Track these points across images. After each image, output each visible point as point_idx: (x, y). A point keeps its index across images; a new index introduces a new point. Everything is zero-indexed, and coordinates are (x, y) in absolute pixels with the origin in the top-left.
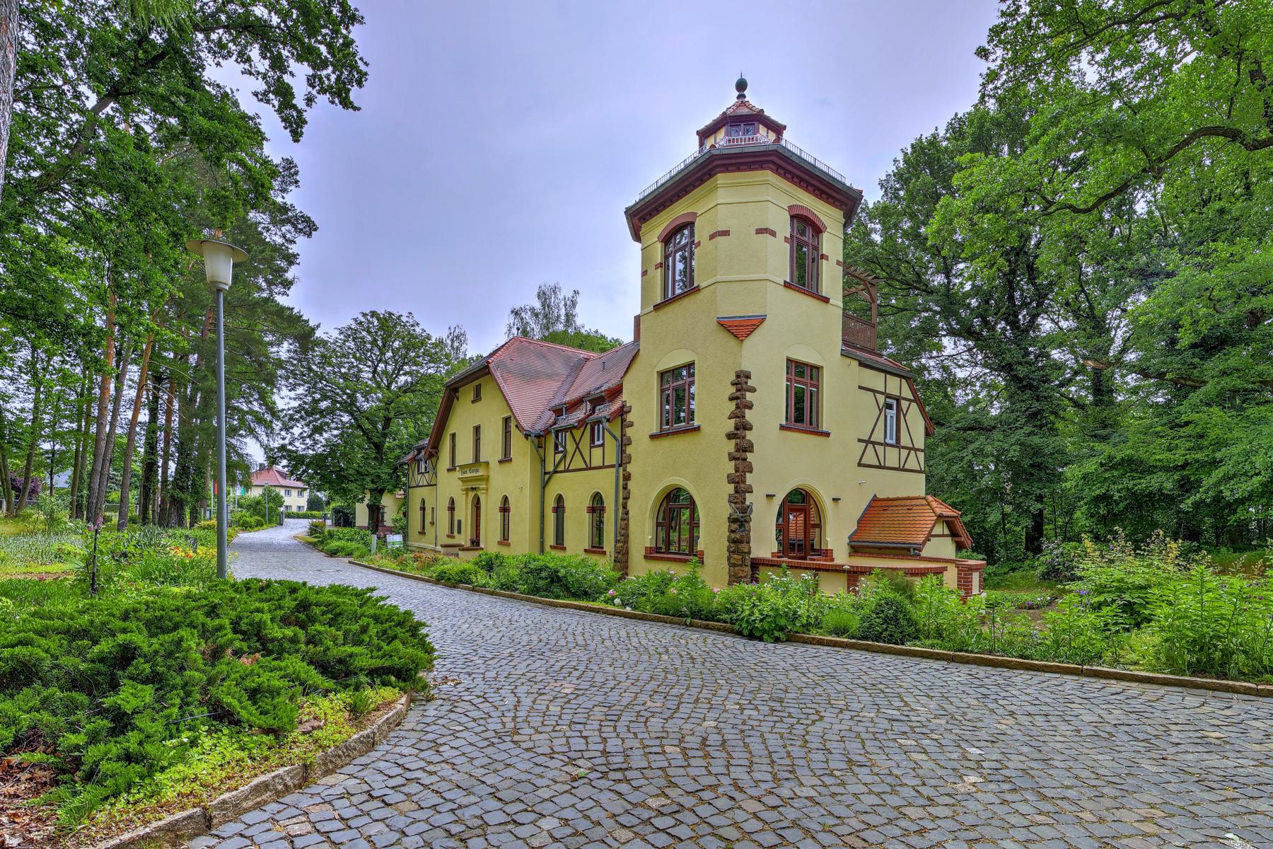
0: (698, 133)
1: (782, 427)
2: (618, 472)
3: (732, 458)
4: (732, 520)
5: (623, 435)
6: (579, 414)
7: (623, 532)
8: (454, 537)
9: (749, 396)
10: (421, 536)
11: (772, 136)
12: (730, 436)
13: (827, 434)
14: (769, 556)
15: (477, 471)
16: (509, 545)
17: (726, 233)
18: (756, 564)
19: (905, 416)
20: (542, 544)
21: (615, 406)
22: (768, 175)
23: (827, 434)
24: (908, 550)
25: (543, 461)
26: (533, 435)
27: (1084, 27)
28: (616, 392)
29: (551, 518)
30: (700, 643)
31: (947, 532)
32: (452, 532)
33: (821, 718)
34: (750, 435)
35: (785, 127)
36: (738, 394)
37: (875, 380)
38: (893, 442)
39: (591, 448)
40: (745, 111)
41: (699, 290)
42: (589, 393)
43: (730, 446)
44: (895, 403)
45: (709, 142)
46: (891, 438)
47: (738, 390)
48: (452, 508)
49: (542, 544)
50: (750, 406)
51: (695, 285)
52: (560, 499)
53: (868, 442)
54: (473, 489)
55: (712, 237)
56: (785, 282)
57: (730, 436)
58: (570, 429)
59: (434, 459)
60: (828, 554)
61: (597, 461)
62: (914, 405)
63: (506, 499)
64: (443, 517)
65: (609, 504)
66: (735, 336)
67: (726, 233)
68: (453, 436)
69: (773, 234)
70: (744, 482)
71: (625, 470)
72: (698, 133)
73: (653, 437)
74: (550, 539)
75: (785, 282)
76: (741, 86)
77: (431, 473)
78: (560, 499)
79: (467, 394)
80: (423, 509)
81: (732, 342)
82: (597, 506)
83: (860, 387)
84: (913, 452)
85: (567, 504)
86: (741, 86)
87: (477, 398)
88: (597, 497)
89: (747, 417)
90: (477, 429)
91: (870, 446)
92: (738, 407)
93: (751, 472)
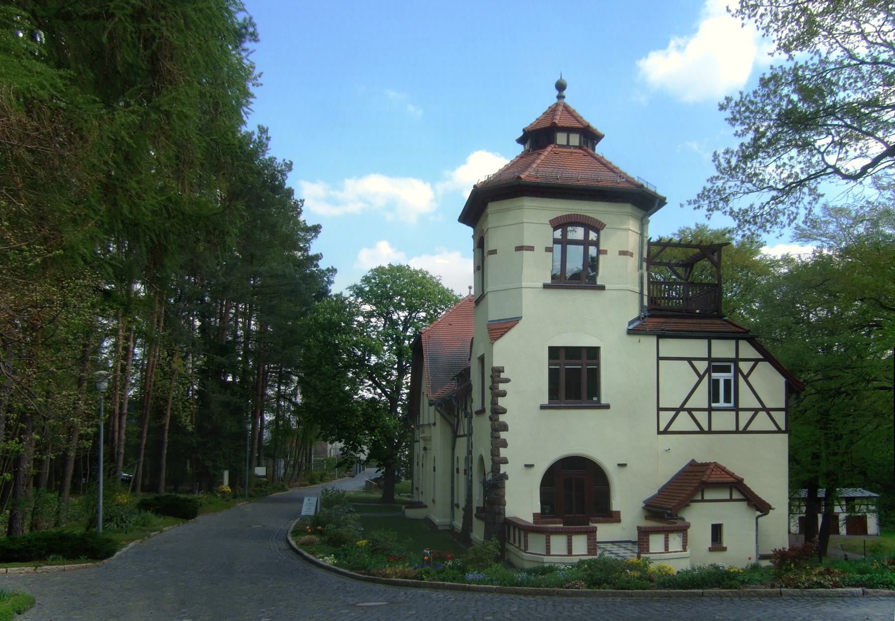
1: (543, 407)
9: (502, 387)
13: (607, 407)
23: (607, 407)
38: (731, 405)
46: (727, 400)
50: (504, 394)
76: (561, 87)
86: (561, 87)
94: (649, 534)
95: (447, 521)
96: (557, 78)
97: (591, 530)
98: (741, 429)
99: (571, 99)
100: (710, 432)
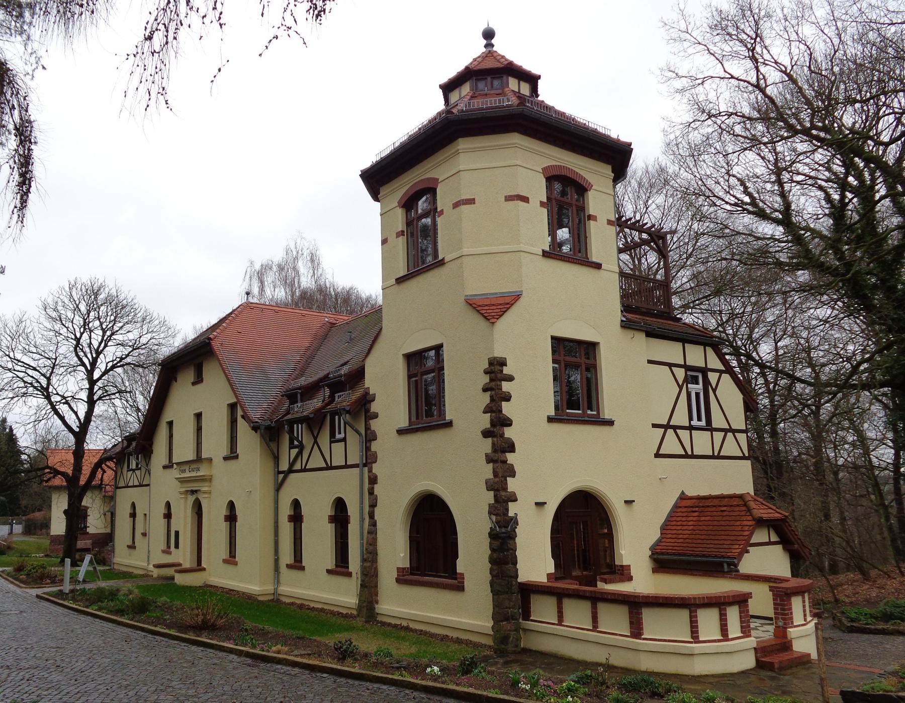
0: (441, 87)
1: (550, 420)
3: (489, 460)
4: (493, 535)
5: (367, 428)
6: (316, 403)
7: (371, 548)
8: (170, 553)
9: (506, 386)
10: (132, 551)
11: (525, 89)
12: (486, 434)
13: (610, 423)
14: (543, 579)
15: (198, 470)
16: (236, 564)
17: (471, 201)
18: (529, 590)
19: (714, 391)
20: (277, 561)
21: (358, 393)
22: (516, 139)
23: (610, 423)
24: (721, 564)
25: (276, 458)
26: (263, 428)
27: (703, 121)
28: (358, 375)
29: (286, 528)
31: (774, 538)
32: (169, 547)
34: (508, 433)
35: (539, 77)
36: (493, 383)
37: (671, 351)
38: (703, 423)
39: (331, 442)
41: (444, 264)
42: (326, 377)
43: (487, 445)
45: (454, 97)
46: (699, 419)
47: (491, 380)
48: (168, 516)
49: (277, 561)
50: (508, 398)
51: (440, 258)
52: (296, 504)
53: (666, 427)
54: (193, 492)
55: (456, 205)
56: (543, 251)
57: (486, 434)
60: (624, 574)
63: (231, 506)
64: (158, 525)
65: (353, 510)
66: (485, 317)
67: (471, 201)
68: (170, 424)
69: (525, 199)
70: (505, 489)
71: (370, 471)
72: (441, 87)
73: (401, 432)
74: (287, 556)
75: (543, 251)
76: (489, 35)
77: (143, 470)
78: (296, 504)
79: (186, 378)
80: (133, 515)
83: (650, 362)
84: (730, 435)
85: (304, 511)
86: (489, 35)
87: (199, 380)
88: (340, 505)
90: (199, 416)
91: (670, 432)
92: (492, 399)
94: (641, 608)
95: (270, 588)
96: (484, 26)
97: (692, 602)
98: (716, 454)
99: (501, 46)
100: (693, 456)
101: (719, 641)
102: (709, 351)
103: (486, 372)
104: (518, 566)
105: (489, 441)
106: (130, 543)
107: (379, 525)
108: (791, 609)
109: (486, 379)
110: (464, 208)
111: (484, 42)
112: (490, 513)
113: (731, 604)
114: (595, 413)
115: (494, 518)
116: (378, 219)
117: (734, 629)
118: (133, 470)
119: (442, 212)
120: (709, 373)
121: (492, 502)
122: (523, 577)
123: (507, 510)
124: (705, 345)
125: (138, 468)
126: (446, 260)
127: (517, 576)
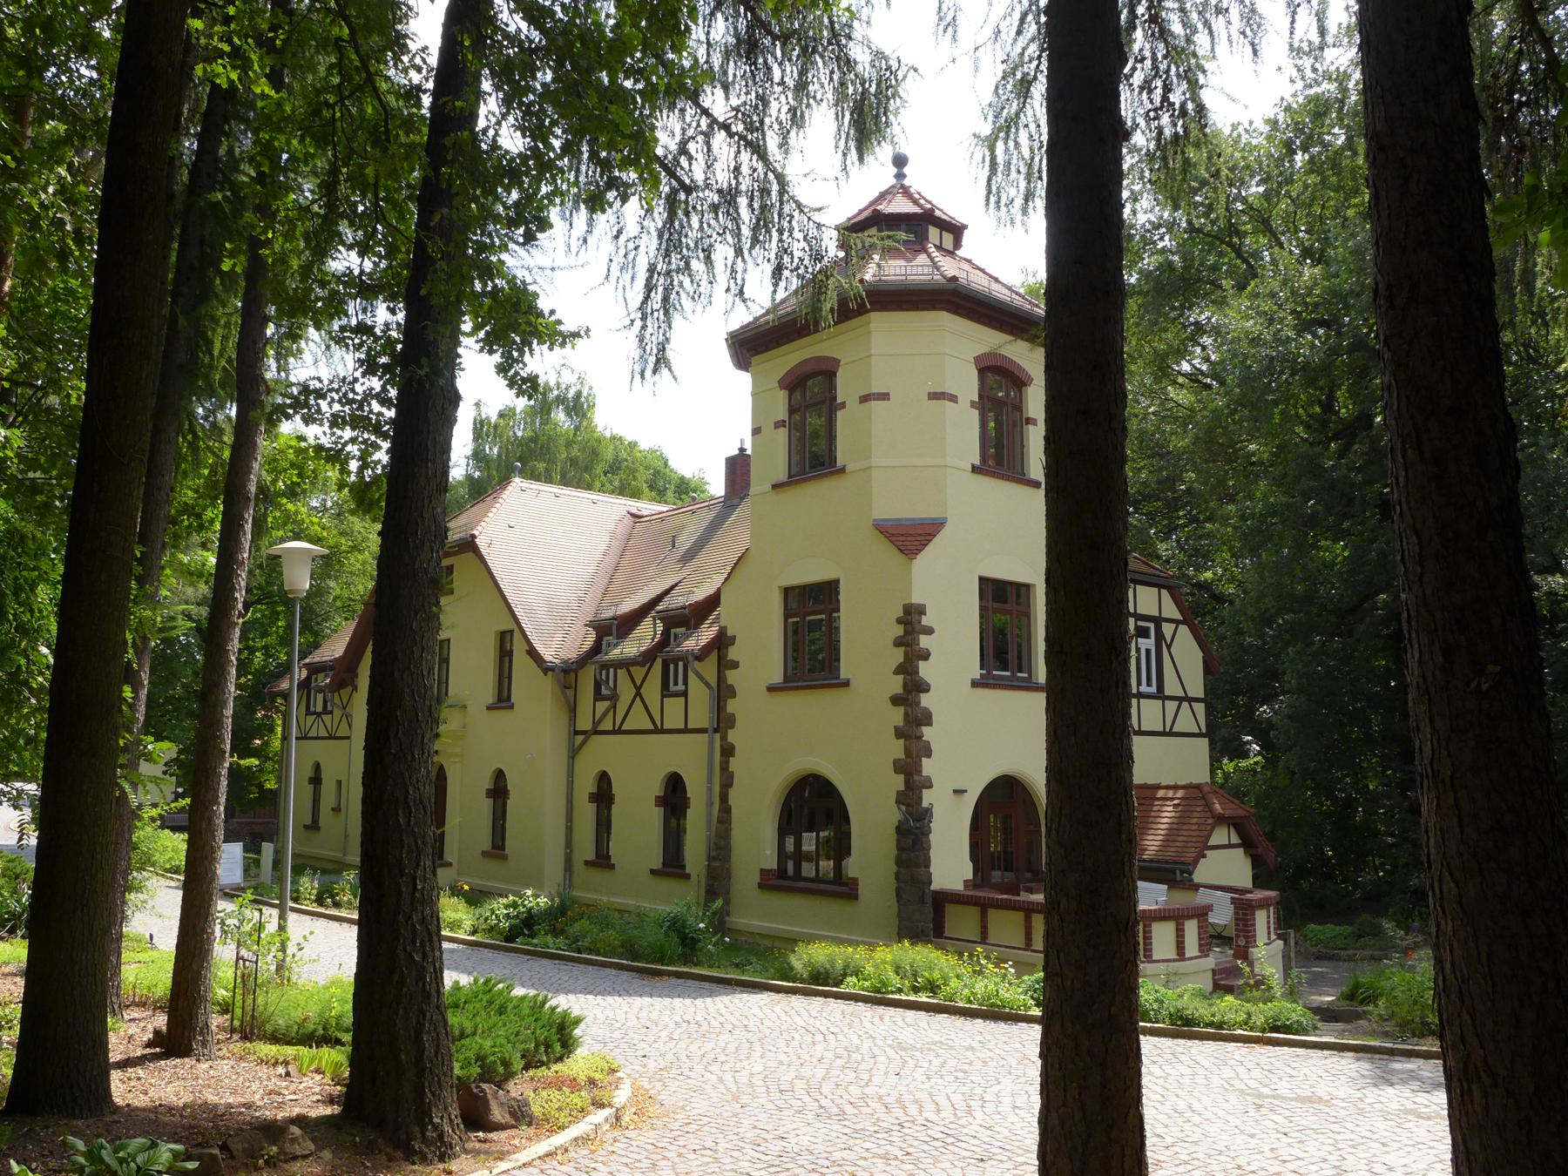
1: (975, 684)
2: (711, 743)
3: (899, 733)
7: (722, 842)
9: (924, 641)
12: (896, 700)
16: (505, 858)
17: (885, 397)
18: (943, 900)
19: (1169, 647)
21: (706, 634)
25: (573, 710)
29: (586, 813)
30: (876, 1020)
31: (1235, 839)
33: (999, 1083)
34: (926, 700)
35: (965, 227)
38: (1153, 689)
39: (663, 697)
40: (900, 206)
43: (897, 716)
44: (1152, 626)
47: (906, 632)
52: (604, 779)
55: (865, 399)
57: (896, 700)
58: (626, 664)
59: (345, 692)
61: (674, 719)
62: (1183, 629)
65: (695, 789)
67: (885, 397)
69: (953, 399)
70: (919, 772)
71: (724, 738)
73: (772, 689)
77: (337, 713)
78: (604, 779)
81: (897, 558)
82: (674, 796)
84: (1185, 705)
89: (922, 674)
93: (929, 755)
101: (1175, 960)
102: (1165, 593)
103: (899, 621)
104: (932, 870)
105: (900, 710)
106: (309, 821)
107: (735, 813)
108: (1254, 925)
109: (899, 630)
110: (875, 405)
111: (895, 170)
112: (898, 802)
113: (1190, 917)
114: (1025, 675)
115: (904, 808)
116: (749, 399)
117: (1192, 948)
118: (319, 715)
119: (843, 405)
120: (1164, 625)
121: (902, 788)
122: (936, 885)
123: (921, 798)
124: (1160, 586)
125: (325, 711)
126: (848, 469)
127: (930, 883)
